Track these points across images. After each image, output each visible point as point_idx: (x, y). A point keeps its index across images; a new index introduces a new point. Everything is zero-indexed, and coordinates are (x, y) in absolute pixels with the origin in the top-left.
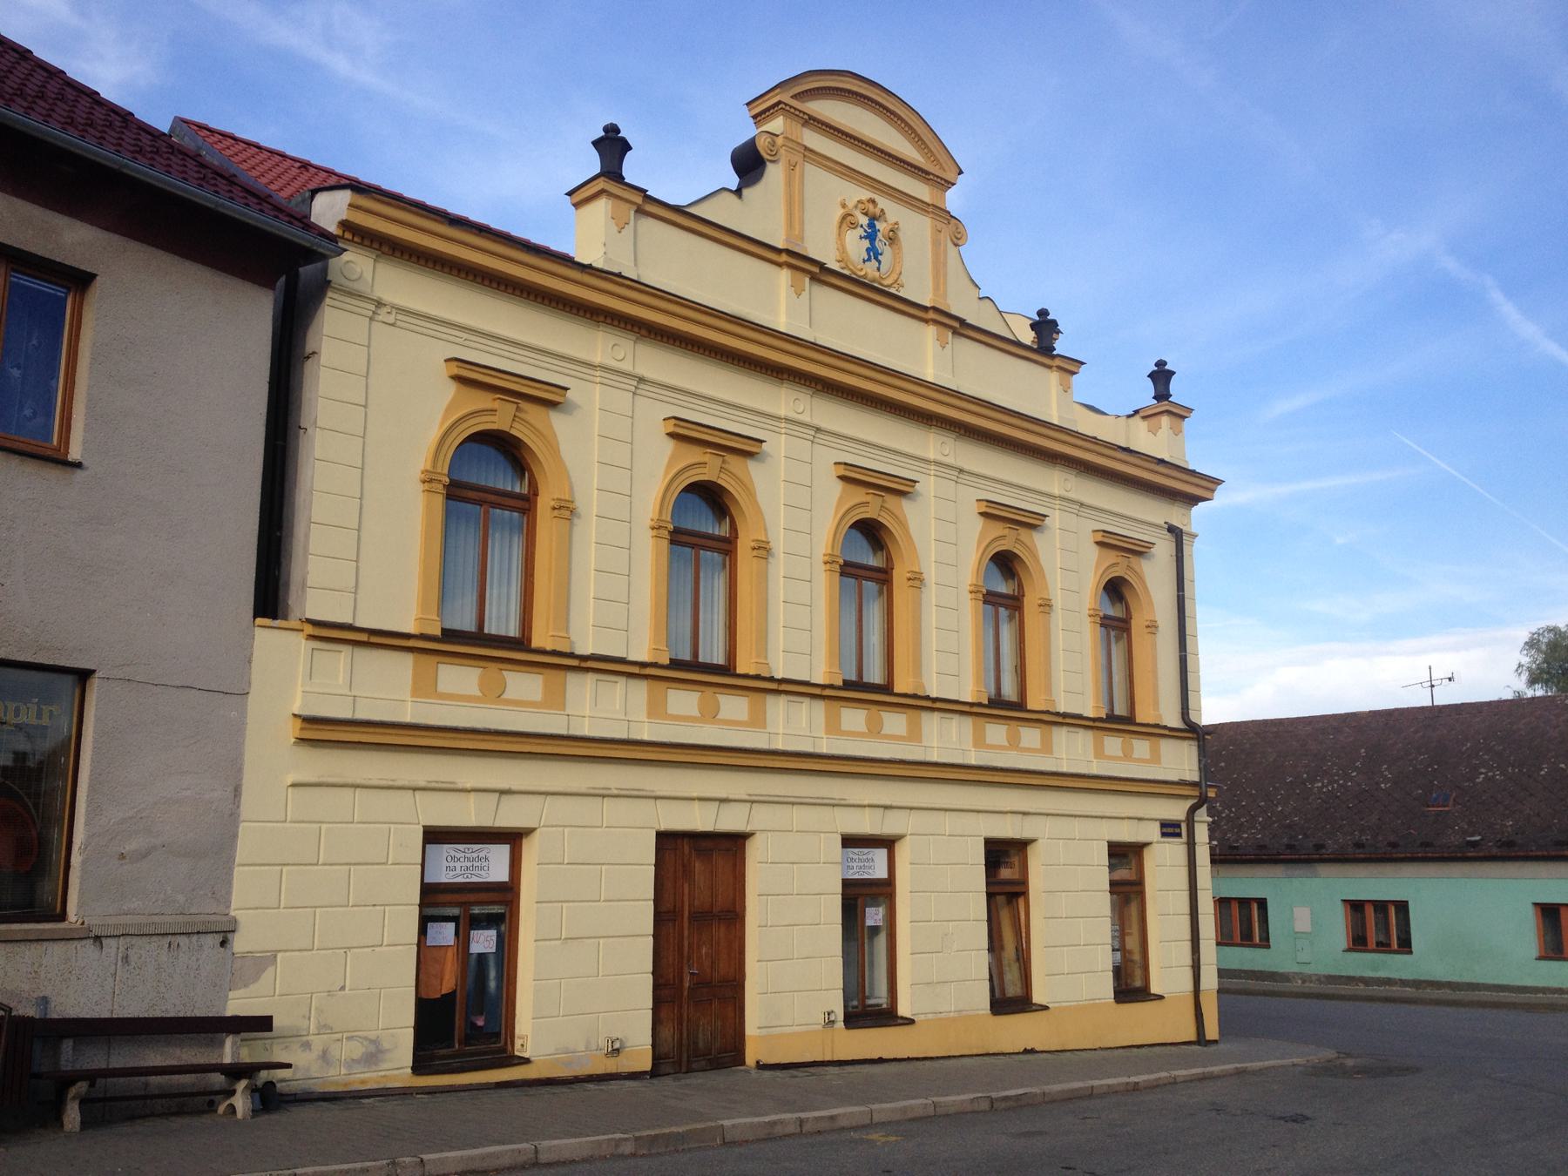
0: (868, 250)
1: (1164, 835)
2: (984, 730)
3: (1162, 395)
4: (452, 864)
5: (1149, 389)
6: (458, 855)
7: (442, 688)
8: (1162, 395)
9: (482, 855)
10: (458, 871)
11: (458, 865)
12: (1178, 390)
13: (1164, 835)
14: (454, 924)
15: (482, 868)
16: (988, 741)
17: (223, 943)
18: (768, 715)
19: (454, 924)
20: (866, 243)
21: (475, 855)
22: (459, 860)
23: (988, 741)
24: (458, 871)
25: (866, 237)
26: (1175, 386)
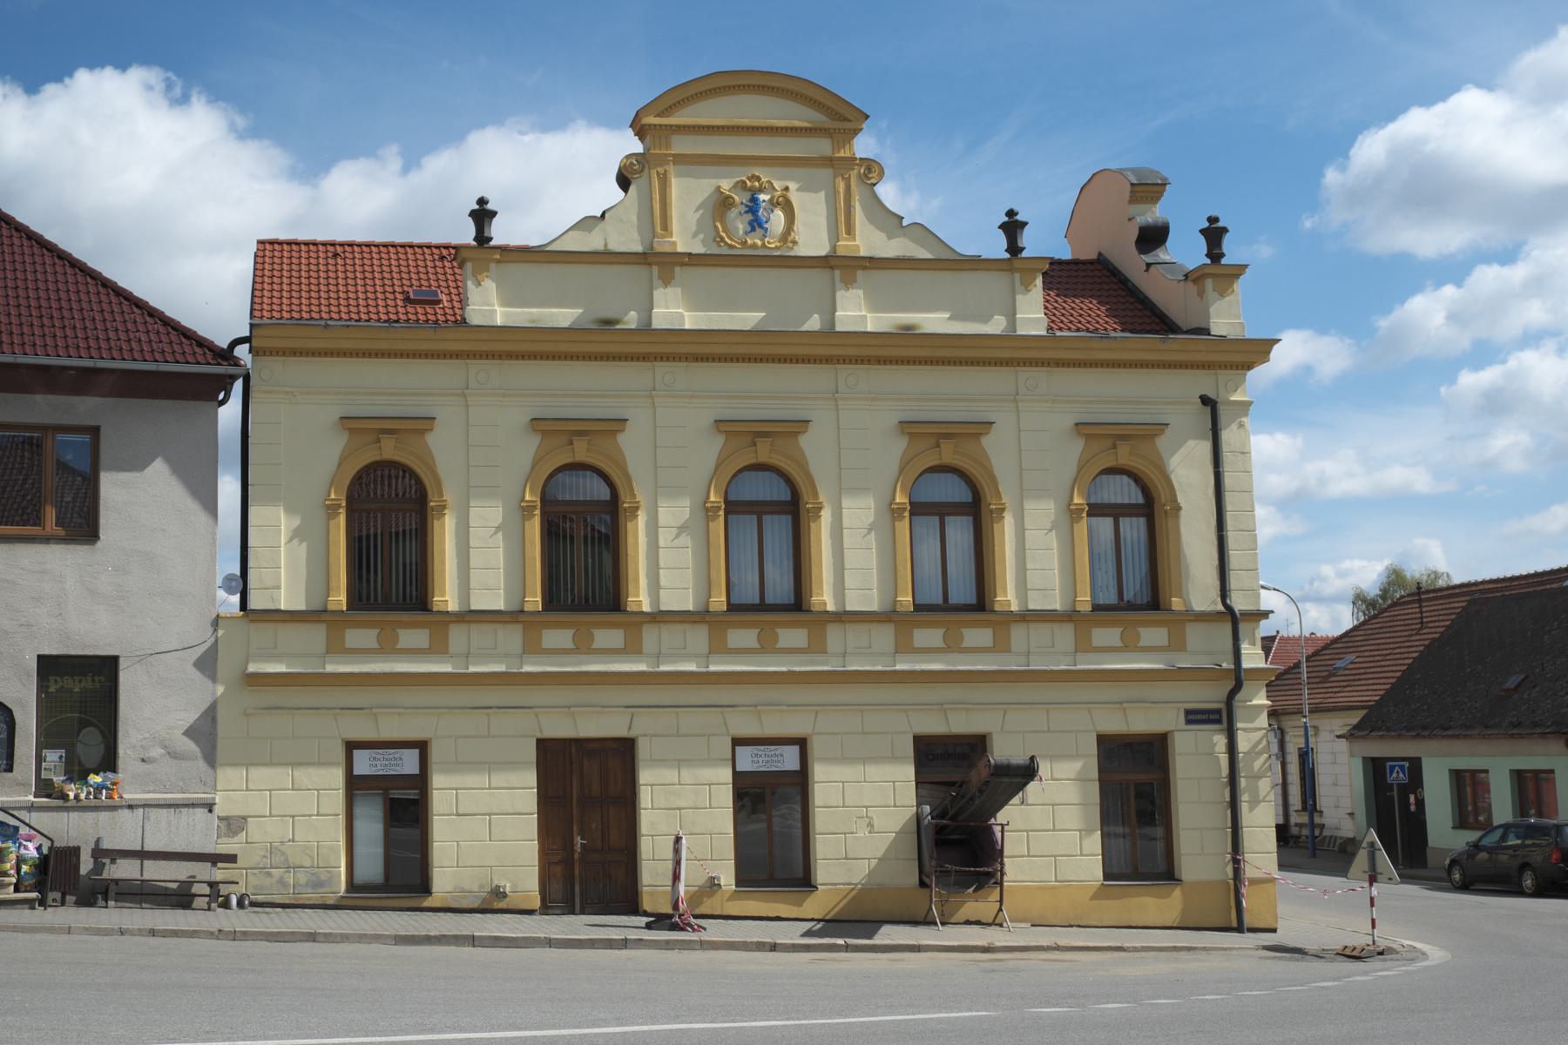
0: (751, 223)
1: (1188, 722)
2: (912, 636)
3: (1215, 254)
4: (374, 763)
5: (1201, 245)
6: (378, 757)
7: (348, 645)
8: (1215, 254)
9: (397, 756)
10: (379, 767)
11: (760, 759)
12: (1232, 252)
13: (1188, 722)
14: (355, 773)
15: (398, 765)
16: (916, 645)
17: (210, 811)
18: (959, 518)
19: (355, 773)
20: (750, 217)
21: (391, 756)
22: (761, 756)
23: (916, 645)
24: (379, 767)
25: (747, 212)
26: (1228, 244)
